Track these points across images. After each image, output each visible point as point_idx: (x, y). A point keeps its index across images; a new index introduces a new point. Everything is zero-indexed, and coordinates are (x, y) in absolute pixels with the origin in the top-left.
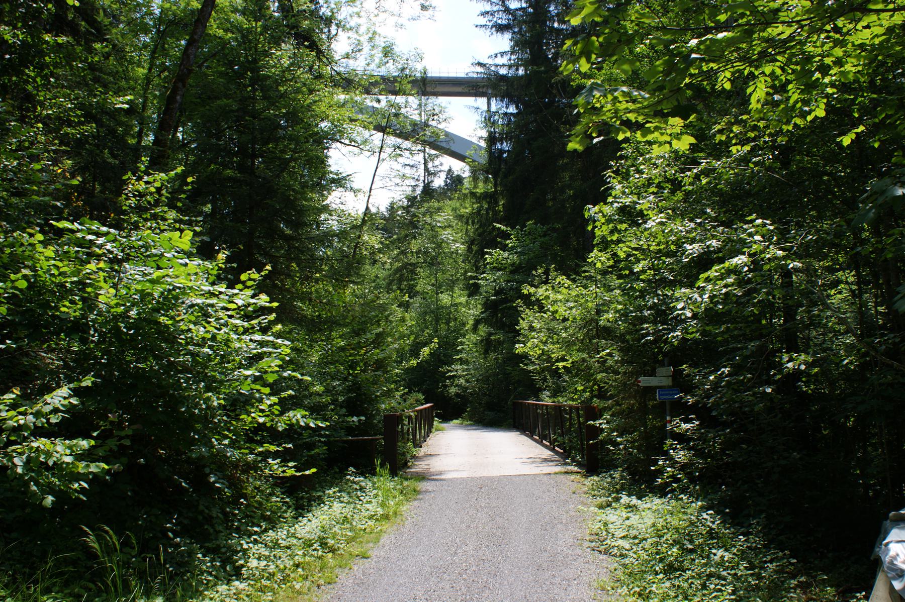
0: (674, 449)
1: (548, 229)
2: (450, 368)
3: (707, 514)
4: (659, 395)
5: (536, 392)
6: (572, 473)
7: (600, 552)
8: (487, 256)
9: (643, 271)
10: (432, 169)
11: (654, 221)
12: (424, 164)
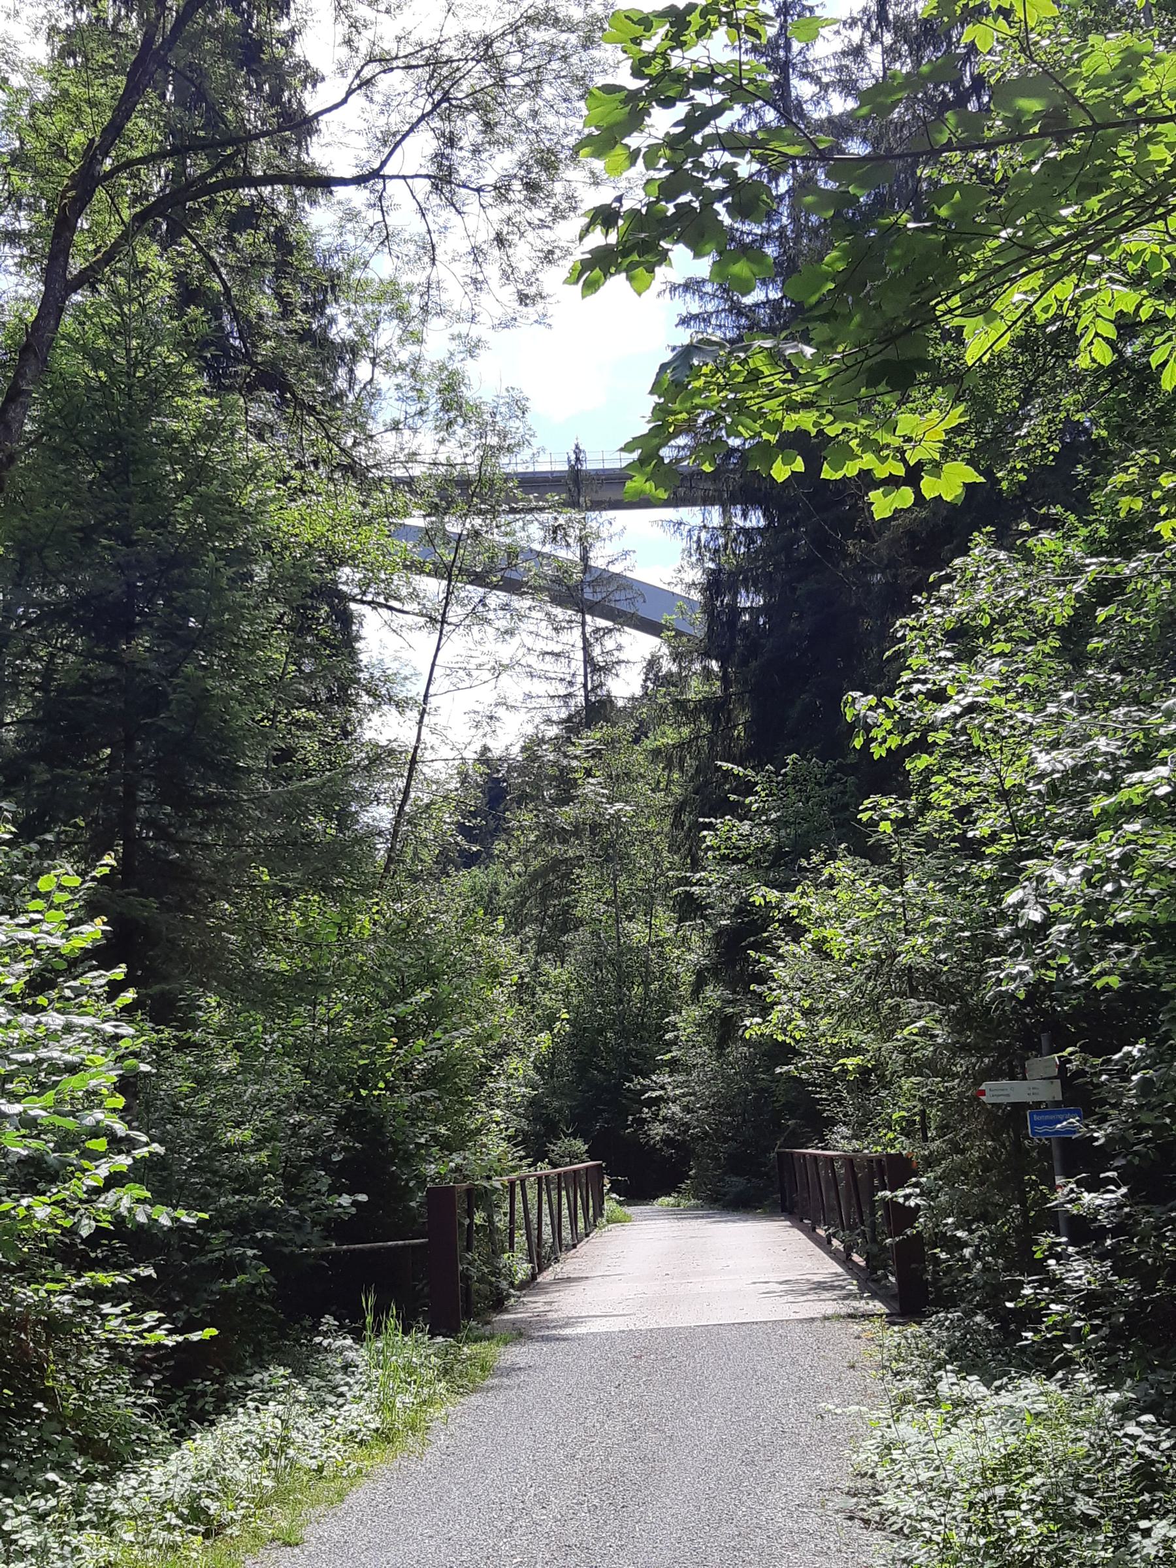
0: (1058, 1257)
1: (838, 768)
2: (647, 1082)
3: (1138, 1424)
4: (1033, 1123)
5: (819, 1126)
6: (867, 1316)
7: (866, 1522)
8: (705, 833)
9: (994, 838)
10: (600, 659)
12: (584, 648)
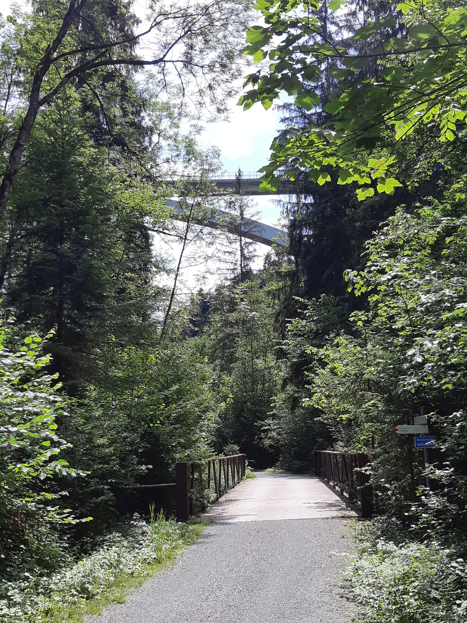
0: (426, 495)
2: (263, 423)
3: (457, 562)
4: (417, 442)
5: (331, 442)
7: (348, 599)
8: (288, 324)
9: (403, 329)
10: (247, 254)
11: (389, 275)
12: (241, 250)
